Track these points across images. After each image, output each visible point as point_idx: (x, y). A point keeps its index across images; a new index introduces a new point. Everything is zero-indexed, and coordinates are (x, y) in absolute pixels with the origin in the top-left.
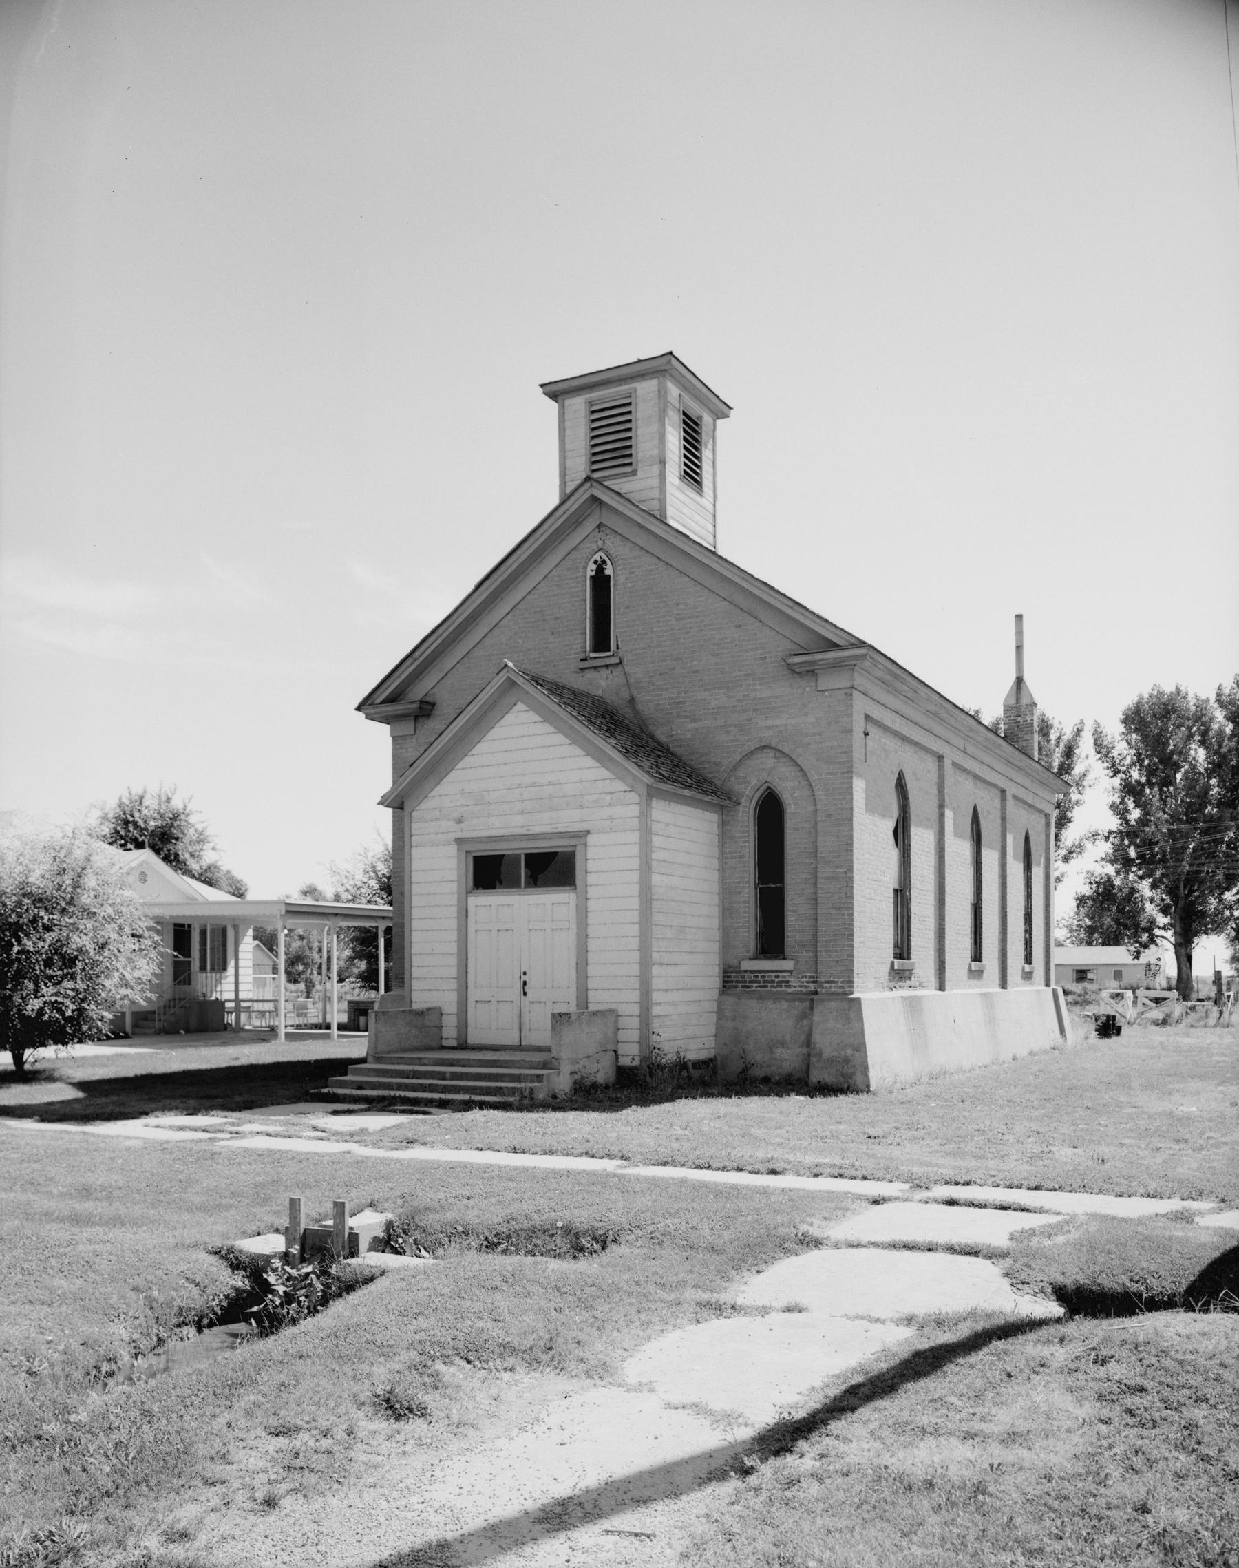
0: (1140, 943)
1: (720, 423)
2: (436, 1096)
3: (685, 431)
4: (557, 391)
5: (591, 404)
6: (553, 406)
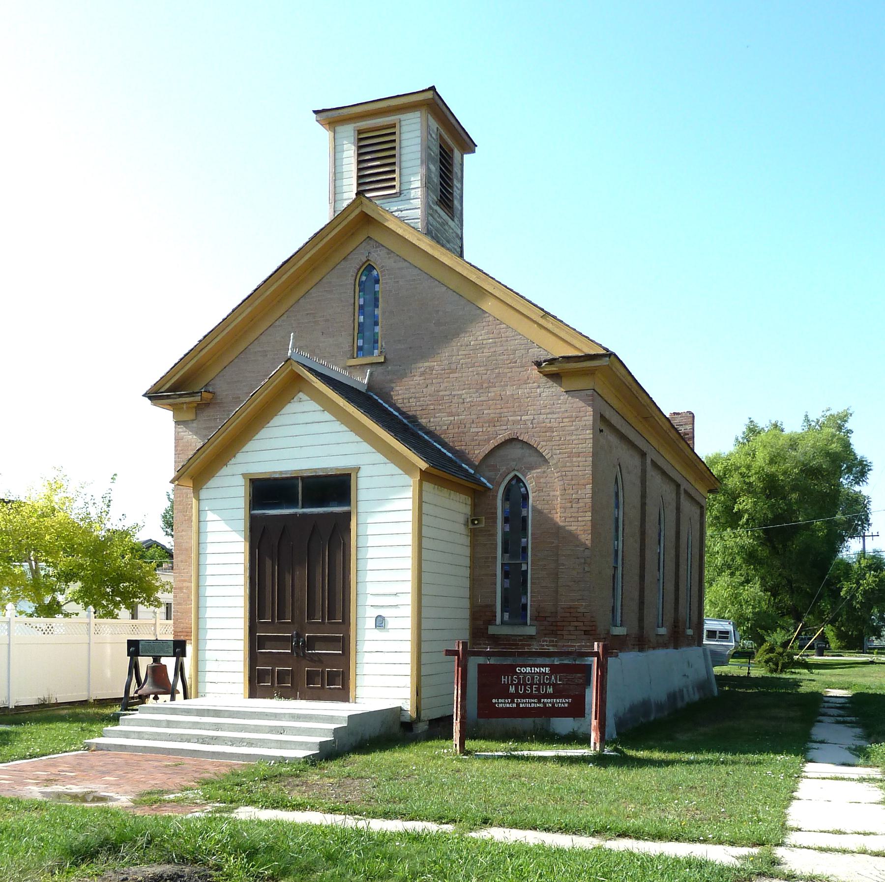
0: (391, 866)
1: (466, 157)
2: (91, 711)
3: (441, 169)
4: (331, 118)
5: (360, 132)
6: (324, 135)
